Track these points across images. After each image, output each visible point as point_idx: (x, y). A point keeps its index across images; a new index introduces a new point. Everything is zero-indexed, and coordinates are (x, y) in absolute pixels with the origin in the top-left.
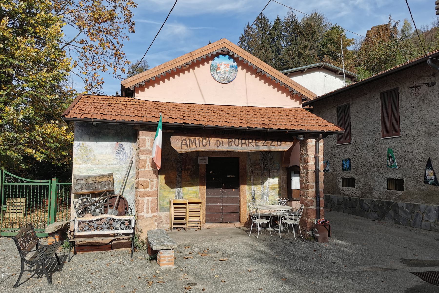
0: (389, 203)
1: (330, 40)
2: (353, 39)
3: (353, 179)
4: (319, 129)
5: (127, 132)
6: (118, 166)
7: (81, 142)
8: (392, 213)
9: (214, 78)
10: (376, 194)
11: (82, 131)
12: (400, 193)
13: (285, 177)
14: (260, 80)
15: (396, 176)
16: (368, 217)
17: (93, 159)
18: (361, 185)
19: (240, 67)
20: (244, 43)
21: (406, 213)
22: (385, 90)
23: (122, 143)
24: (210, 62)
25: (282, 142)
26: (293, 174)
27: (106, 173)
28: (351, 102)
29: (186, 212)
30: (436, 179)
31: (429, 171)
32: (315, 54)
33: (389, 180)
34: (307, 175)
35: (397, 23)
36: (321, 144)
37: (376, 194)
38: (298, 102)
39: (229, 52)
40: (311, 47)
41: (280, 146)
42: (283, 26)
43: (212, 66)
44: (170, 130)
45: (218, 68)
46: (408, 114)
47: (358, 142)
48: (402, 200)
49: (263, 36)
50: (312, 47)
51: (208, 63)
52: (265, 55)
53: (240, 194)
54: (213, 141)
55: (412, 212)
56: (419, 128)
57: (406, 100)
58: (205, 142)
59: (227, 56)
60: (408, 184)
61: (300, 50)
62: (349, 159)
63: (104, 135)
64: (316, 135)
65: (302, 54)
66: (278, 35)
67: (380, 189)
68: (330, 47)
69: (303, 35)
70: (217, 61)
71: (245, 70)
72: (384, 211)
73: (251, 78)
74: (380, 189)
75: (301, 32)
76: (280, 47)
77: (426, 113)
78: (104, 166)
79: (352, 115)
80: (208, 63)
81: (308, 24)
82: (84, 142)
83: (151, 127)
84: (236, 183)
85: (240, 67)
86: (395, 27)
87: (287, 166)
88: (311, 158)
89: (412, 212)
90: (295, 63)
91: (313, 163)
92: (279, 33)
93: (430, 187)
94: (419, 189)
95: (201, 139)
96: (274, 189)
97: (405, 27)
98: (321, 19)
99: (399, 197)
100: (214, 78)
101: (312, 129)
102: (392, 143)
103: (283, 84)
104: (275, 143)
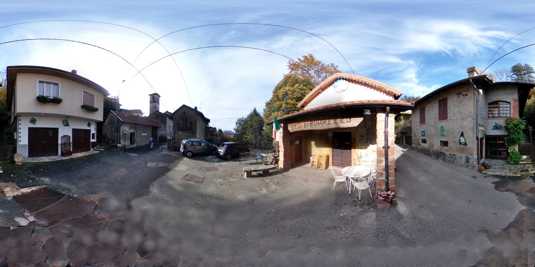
0: (441, 152)
12: (446, 148)
15: (445, 140)
25: (352, 119)
30: (465, 142)
31: (462, 139)
33: (441, 141)
41: (349, 122)
46: (452, 109)
67: (437, 146)
84: (350, 149)
88: (381, 134)
89: (452, 157)
91: (383, 138)
93: (462, 146)
96: (374, 151)
99: (446, 150)
102: (443, 123)
104: (345, 120)
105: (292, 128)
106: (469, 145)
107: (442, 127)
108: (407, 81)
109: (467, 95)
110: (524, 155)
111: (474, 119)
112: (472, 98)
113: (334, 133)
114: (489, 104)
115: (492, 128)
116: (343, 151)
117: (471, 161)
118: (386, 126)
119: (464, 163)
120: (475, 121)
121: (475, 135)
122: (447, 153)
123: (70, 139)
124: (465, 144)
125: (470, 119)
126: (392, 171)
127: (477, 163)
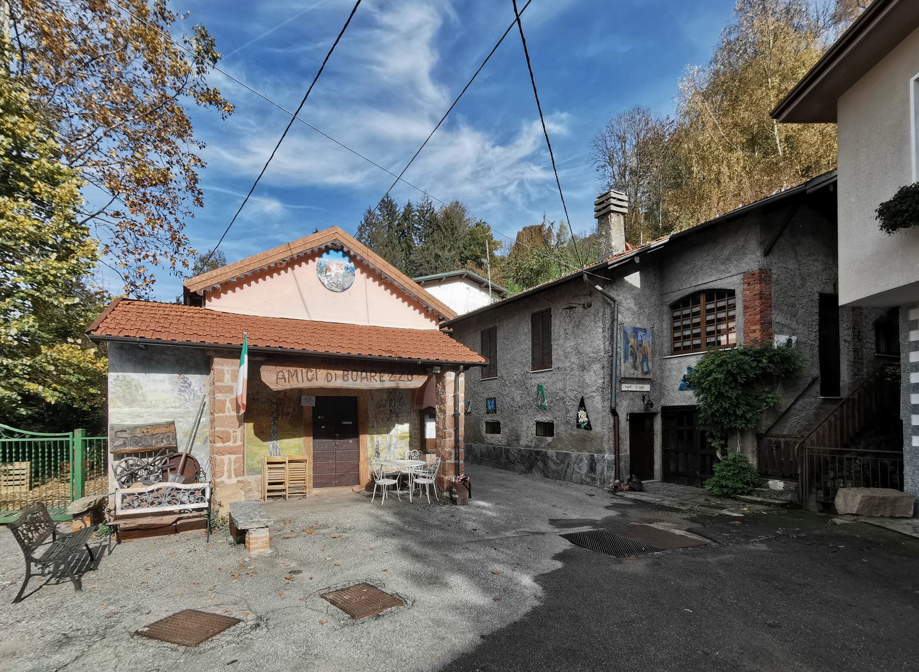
0: (537, 453)
1: (474, 240)
3: (498, 423)
4: (459, 360)
5: (195, 358)
6: (182, 410)
7: (121, 374)
9: (323, 284)
10: (524, 442)
11: (121, 356)
12: (549, 439)
13: (417, 422)
16: (514, 470)
17: (140, 400)
18: (507, 430)
21: (556, 463)
22: (536, 310)
23: (187, 376)
26: (427, 418)
27: (164, 420)
28: (497, 324)
29: (284, 474)
30: (589, 422)
31: (582, 414)
36: (462, 379)
37: (524, 442)
43: (320, 265)
44: (262, 357)
45: (328, 269)
46: (561, 341)
48: (552, 448)
51: (314, 261)
53: (359, 447)
54: (322, 373)
55: (562, 462)
56: (573, 360)
57: (559, 326)
58: (310, 374)
60: (559, 429)
63: (158, 362)
64: (455, 367)
67: (528, 435)
70: (325, 259)
72: (532, 462)
74: (528, 435)
75: (438, 226)
78: (160, 410)
80: (314, 261)
81: (447, 215)
83: (233, 353)
85: (359, 270)
87: (420, 408)
89: (562, 462)
94: (571, 434)
95: (304, 370)
99: (549, 445)
100: (323, 284)
101: (451, 359)
102: (542, 378)
104: (404, 377)
105: (272, 377)
106: (597, 428)
107: (540, 387)
108: (388, 99)
109: (590, 306)
110: (774, 477)
111: (603, 367)
112: (601, 314)
113: (318, 399)
114: (675, 306)
115: (679, 383)
116: (338, 442)
117: (599, 468)
118: (456, 389)
119: (586, 474)
121: (607, 404)
122: (551, 452)
124: (588, 427)
125: (597, 367)
127: (613, 474)
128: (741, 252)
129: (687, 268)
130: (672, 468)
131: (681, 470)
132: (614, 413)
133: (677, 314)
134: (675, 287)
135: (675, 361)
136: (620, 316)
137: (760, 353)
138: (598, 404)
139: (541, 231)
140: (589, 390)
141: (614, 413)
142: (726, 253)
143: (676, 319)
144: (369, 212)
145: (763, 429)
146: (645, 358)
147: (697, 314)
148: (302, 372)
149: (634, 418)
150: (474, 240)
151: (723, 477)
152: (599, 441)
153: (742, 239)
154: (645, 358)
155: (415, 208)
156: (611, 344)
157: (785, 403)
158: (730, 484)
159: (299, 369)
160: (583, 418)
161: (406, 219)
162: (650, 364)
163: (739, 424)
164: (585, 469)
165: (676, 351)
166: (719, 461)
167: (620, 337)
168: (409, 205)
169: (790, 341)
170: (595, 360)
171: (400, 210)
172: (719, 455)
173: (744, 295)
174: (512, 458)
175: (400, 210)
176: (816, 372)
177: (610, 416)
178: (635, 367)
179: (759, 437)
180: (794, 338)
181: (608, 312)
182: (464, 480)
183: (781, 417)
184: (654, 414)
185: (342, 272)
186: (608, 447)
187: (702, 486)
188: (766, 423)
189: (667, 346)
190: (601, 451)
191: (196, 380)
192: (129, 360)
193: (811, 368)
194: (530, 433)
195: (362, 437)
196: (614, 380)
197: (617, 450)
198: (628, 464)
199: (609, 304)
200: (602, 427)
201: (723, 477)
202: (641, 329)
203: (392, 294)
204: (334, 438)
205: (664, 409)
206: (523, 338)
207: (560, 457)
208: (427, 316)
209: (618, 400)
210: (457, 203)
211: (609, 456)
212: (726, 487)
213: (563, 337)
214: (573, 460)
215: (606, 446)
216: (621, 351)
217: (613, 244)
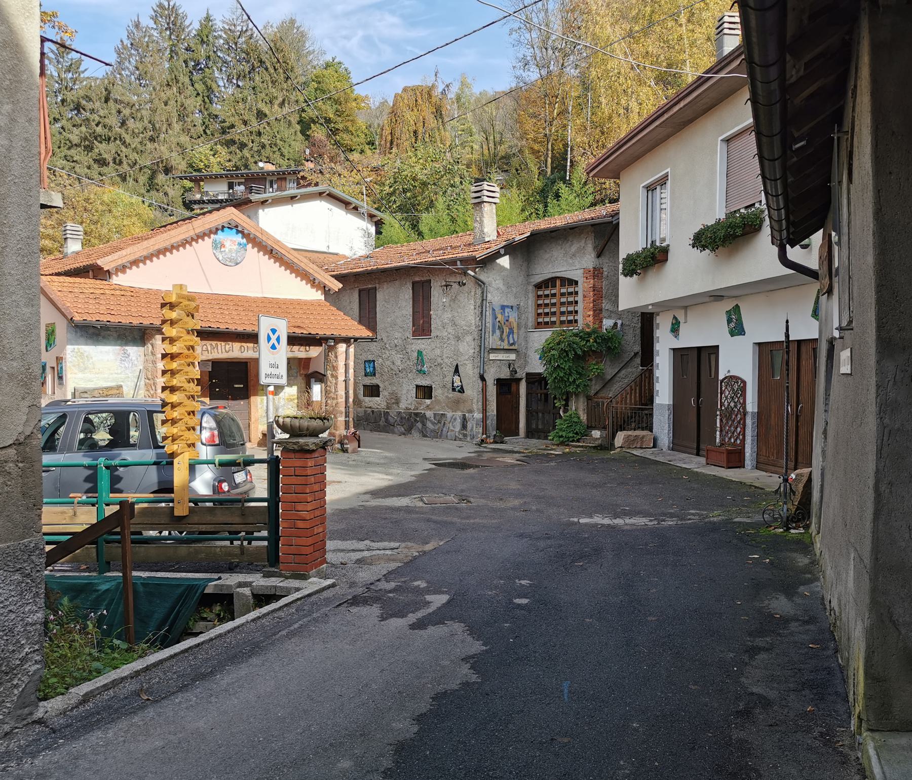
0: (416, 414)
1: (324, 92)
2: (366, 97)
3: (378, 386)
4: (350, 335)
6: (123, 376)
7: (76, 347)
8: (419, 425)
9: (218, 259)
10: (403, 405)
11: (76, 332)
12: (428, 401)
13: (304, 385)
14: (275, 262)
15: (424, 382)
16: (393, 433)
18: (386, 393)
19: (250, 245)
20: (127, 64)
21: (433, 423)
22: (417, 279)
23: (127, 348)
24: (212, 236)
26: (313, 380)
27: (113, 384)
28: (377, 286)
31: (456, 378)
32: (292, 119)
33: (417, 386)
34: (336, 384)
35: (447, 86)
36: (352, 350)
37: (403, 405)
38: (320, 292)
39: (237, 226)
40: (284, 100)
42: (221, 37)
43: (214, 242)
45: (223, 246)
47: (385, 339)
48: (430, 409)
49: (171, 51)
50: (286, 102)
51: (210, 237)
52: (179, 100)
53: (250, 408)
54: (237, 345)
55: (439, 422)
56: (450, 330)
57: (438, 297)
58: (227, 347)
59: (234, 231)
61: (261, 106)
62: (374, 361)
63: (104, 337)
64: (347, 340)
65: (266, 116)
66: (208, 57)
67: (408, 400)
68: (323, 107)
69: (267, 69)
70: (220, 236)
71: (256, 249)
72: (411, 423)
73: (264, 259)
74: (408, 400)
75: (261, 61)
76: (214, 86)
77: (456, 314)
78: (106, 376)
79: (378, 303)
80: (210, 237)
81: (275, 49)
82: (80, 347)
85: (250, 245)
86: (443, 93)
89: (439, 422)
90: (251, 133)
91: (343, 371)
92: (211, 53)
94: (447, 397)
95: (223, 344)
96: (292, 400)
97: (461, 89)
98: (303, 35)
100: (218, 259)
101: (344, 335)
102: (421, 344)
103: (304, 270)
106: (468, 392)
107: (420, 353)
110: (595, 428)
112: (473, 293)
114: (539, 286)
117: (469, 425)
120: (477, 342)
121: (477, 371)
122: (429, 414)
123: (743, 389)
124: (462, 390)
125: (469, 338)
126: (25, 722)
127: (481, 431)
128: (581, 250)
129: (547, 256)
130: (534, 426)
131: (540, 427)
132: (482, 378)
133: (540, 293)
134: (538, 271)
135: (536, 335)
136: (489, 295)
137: (589, 334)
138: (469, 371)
139: (430, 96)
140: (463, 358)
141: (482, 378)
142: (574, 249)
143: (539, 297)
144: (137, 25)
145: (592, 392)
146: (511, 331)
147: (554, 295)
148: (221, 345)
149: (501, 384)
150: (324, 92)
151: (561, 430)
152: (470, 402)
153: (583, 241)
154: (511, 331)
155: (219, 24)
156: (481, 319)
157: (610, 372)
158: (564, 434)
159: (219, 343)
160: (457, 383)
161: (203, 42)
162: (515, 336)
163: (571, 389)
164: (458, 427)
165: (539, 325)
166: (561, 417)
167: (489, 313)
168: (208, 19)
169: (616, 324)
170: (468, 333)
171: (193, 24)
172: (561, 413)
173: (584, 287)
174: (391, 420)
175: (193, 24)
176: (637, 348)
177: (480, 381)
178: (502, 339)
179: (589, 398)
180: (619, 322)
181: (479, 291)
182: (354, 433)
183: (607, 384)
184: (519, 380)
185: (235, 247)
186: (478, 403)
187: (546, 438)
188: (594, 388)
189: (531, 319)
190: (471, 411)
191: (134, 351)
192: (82, 336)
193: (632, 344)
194: (409, 396)
195: (253, 399)
196: (483, 350)
197: (484, 410)
198: (495, 422)
199: (480, 286)
200: (472, 391)
201: (561, 430)
202: (508, 306)
203: (280, 266)
204: (228, 399)
205: (527, 374)
206: (404, 304)
207: (437, 418)
208: (313, 286)
209: (486, 368)
210: (293, 22)
211: (478, 416)
212: (562, 436)
213: (441, 308)
214: (449, 420)
215: (475, 406)
216: (489, 325)
217: (486, 230)
